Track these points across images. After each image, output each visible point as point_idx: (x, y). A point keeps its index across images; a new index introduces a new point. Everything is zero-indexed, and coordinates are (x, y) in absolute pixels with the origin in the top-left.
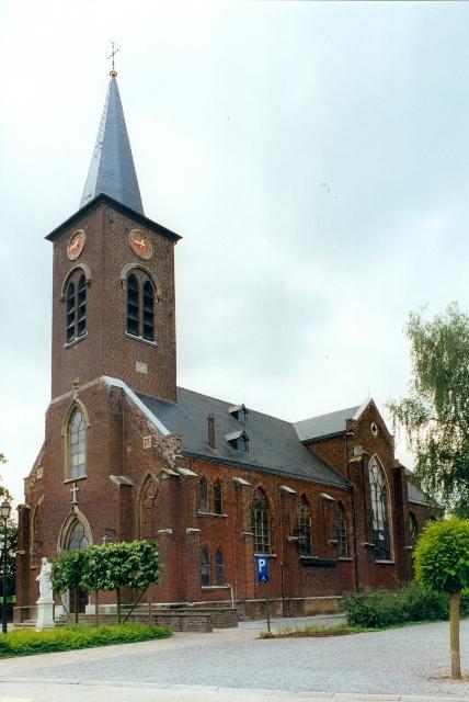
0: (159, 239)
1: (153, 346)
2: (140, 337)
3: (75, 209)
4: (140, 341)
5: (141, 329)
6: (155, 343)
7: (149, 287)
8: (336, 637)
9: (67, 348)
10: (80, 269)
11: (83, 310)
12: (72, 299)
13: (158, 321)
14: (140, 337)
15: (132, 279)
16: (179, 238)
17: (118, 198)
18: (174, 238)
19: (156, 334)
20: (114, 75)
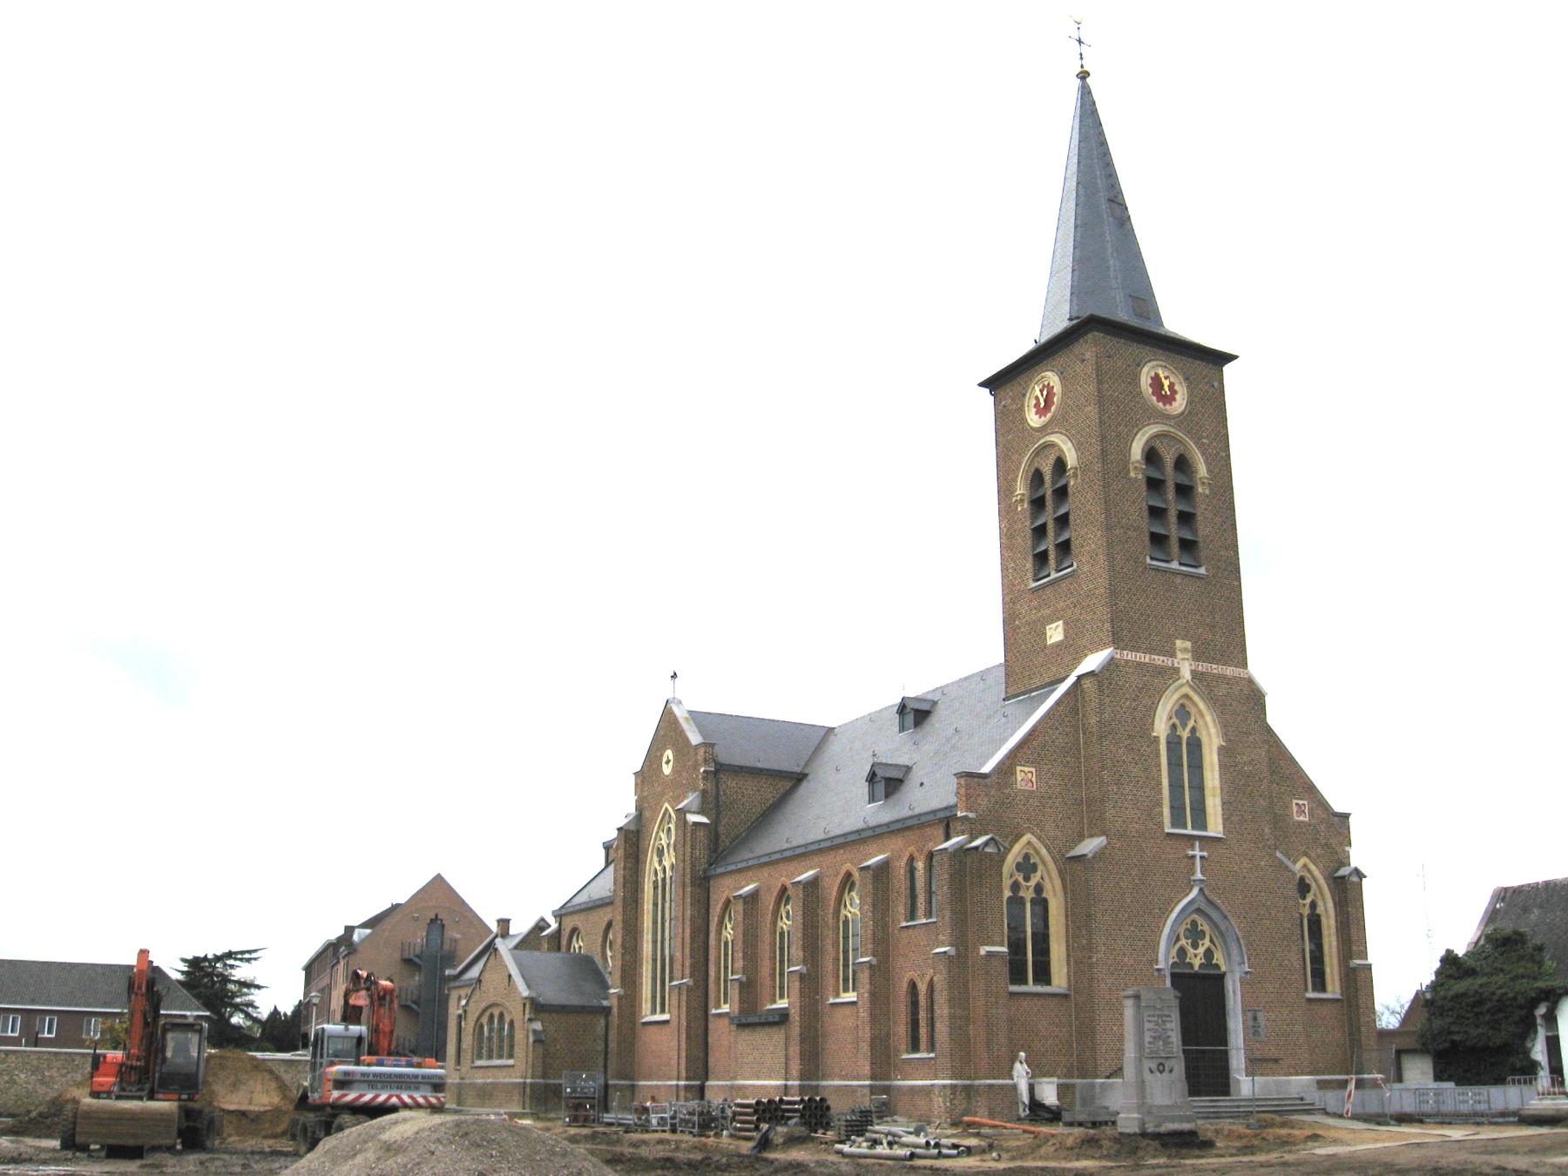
0: (1199, 366)
1: (1198, 577)
2: (1175, 565)
3: (1026, 347)
4: (1175, 573)
5: (1175, 547)
6: (1202, 571)
7: (1182, 464)
8: (742, 763)
9: (1310, 1000)
10: (1053, 445)
11: (1063, 521)
12: (1042, 520)
13: (1204, 529)
14: (1175, 565)
15: (1151, 456)
16: (1229, 358)
17: (1123, 315)
18: (1221, 359)
19: (1203, 553)
20: (1083, 76)
